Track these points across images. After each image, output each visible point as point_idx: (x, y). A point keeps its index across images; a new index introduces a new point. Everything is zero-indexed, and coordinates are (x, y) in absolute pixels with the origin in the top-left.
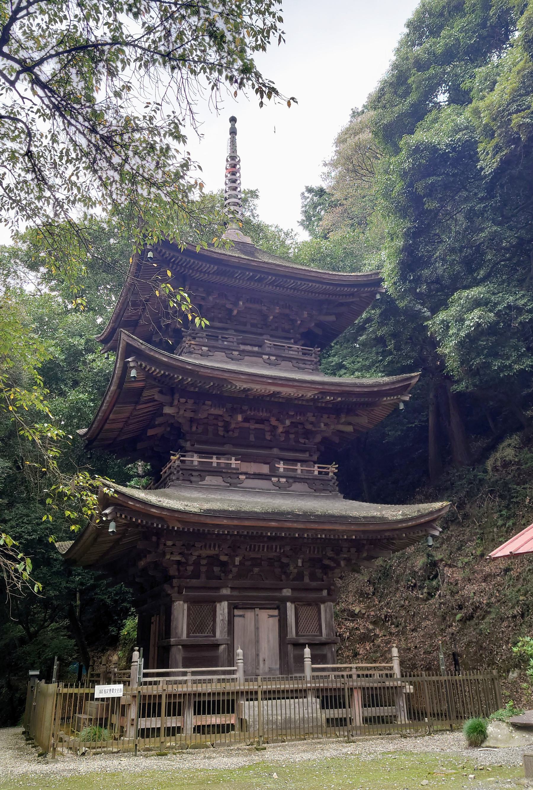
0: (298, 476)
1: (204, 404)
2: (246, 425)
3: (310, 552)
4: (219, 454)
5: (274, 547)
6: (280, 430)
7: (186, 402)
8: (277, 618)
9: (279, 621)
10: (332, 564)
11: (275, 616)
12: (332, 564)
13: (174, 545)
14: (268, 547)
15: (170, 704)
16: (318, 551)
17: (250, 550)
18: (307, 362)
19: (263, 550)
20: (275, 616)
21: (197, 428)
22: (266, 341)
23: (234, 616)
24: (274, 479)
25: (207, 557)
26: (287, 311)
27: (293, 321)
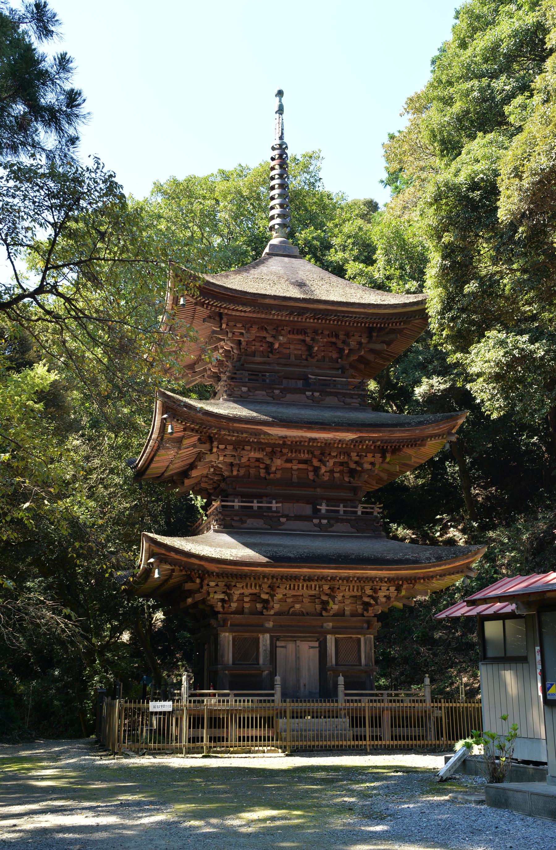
0: (340, 517)
1: (243, 449)
2: (289, 465)
3: (349, 590)
4: (259, 497)
5: (313, 586)
6: (323, 470)
7: (226, 448)
8: (318, 649)
9: (320, 651)
10: (372, 602)
11: (316, 647)
12: (372, 602)
13: (217, 585)
14: (307, 586)
15: (211, 718)
16: (357, 590)
17: (290, 589)
18: (354, 397)
19: (303, 589)
20: (316, 647)
21: (238, 471)
22: (310, 376)
23: (276, 647)
24: (316, 521)
25: (250, 594)
26: (334, 340)
27: (341, 351)
